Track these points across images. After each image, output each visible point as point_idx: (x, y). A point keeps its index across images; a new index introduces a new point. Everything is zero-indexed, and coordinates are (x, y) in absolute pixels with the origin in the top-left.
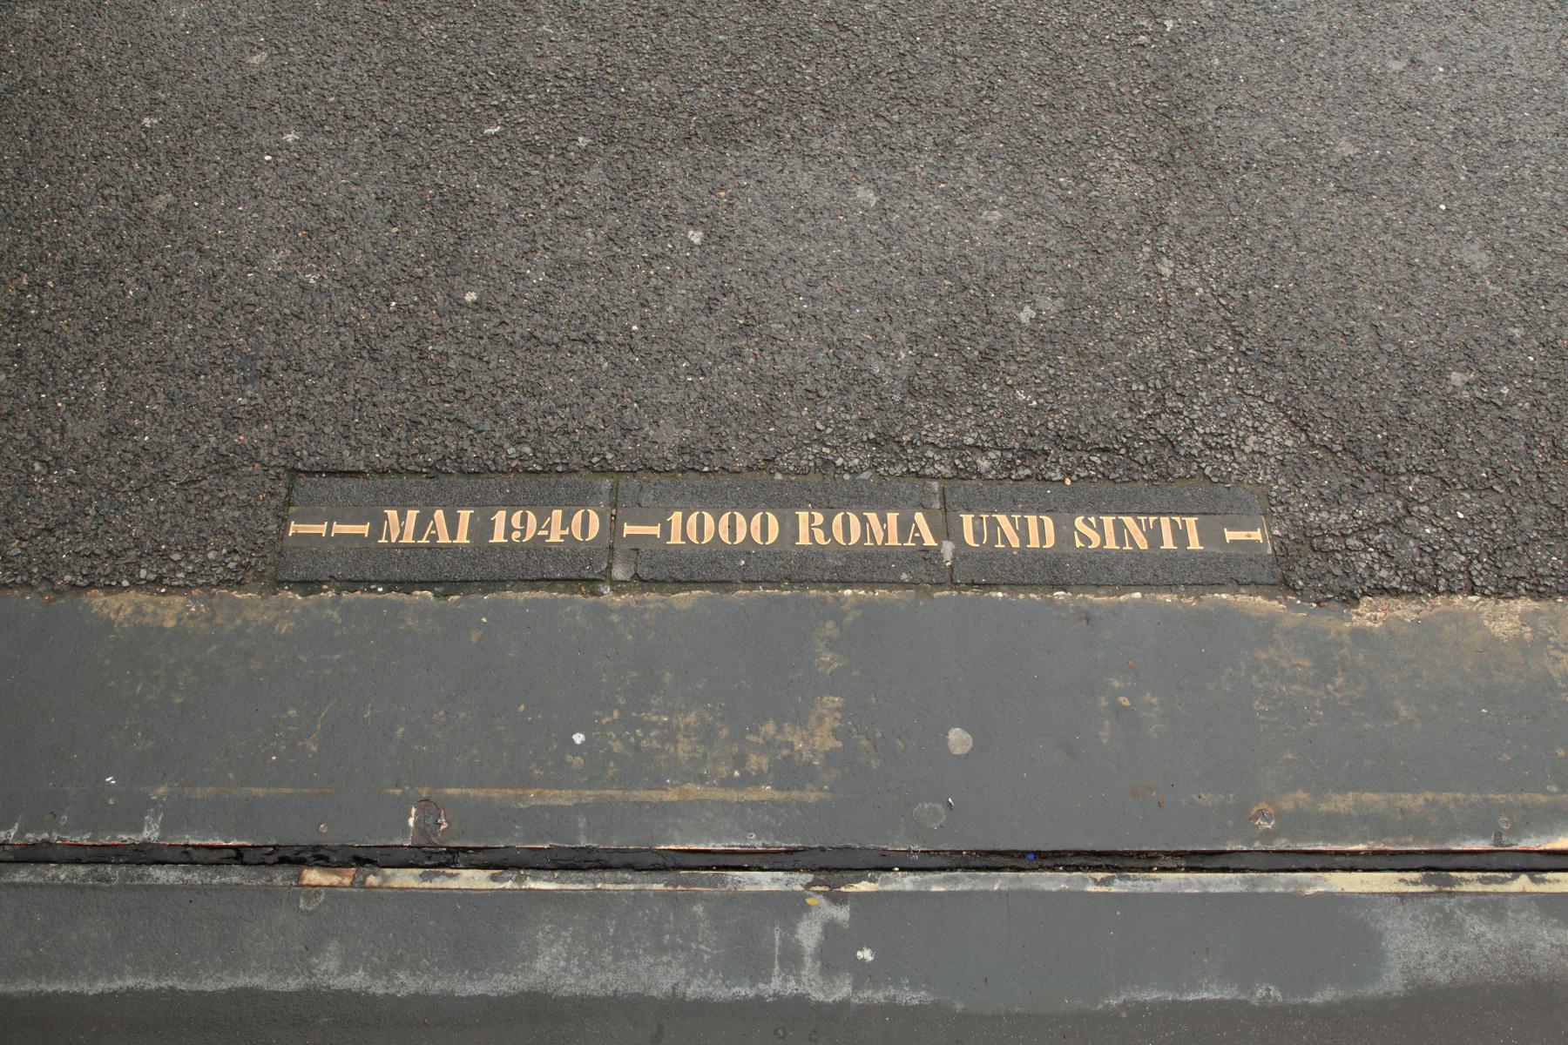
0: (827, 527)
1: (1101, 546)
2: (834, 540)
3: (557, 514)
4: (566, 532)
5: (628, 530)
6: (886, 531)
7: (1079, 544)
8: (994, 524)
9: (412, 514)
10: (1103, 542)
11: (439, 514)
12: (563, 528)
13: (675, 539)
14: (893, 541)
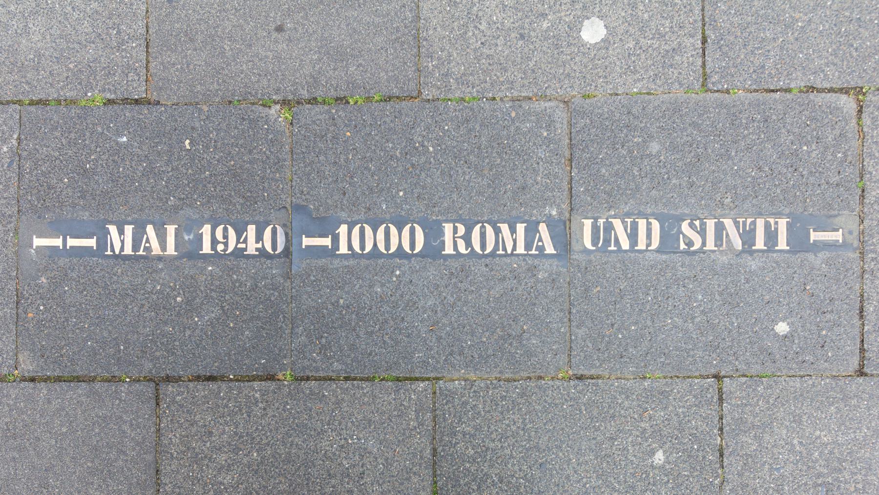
0: (467, 238)
1: (701, 248)
2: (473, 249)
3: (251, 229)
4: (260, 245)
5: (306, 241)
6: (515, 241)
7: (683, 246)
8: (609, 228)
9: (129, 229)
10: (704, 244)
11: (150, 229)
12: (257, 242)
13: (343, 249)
14: (520, 250)
